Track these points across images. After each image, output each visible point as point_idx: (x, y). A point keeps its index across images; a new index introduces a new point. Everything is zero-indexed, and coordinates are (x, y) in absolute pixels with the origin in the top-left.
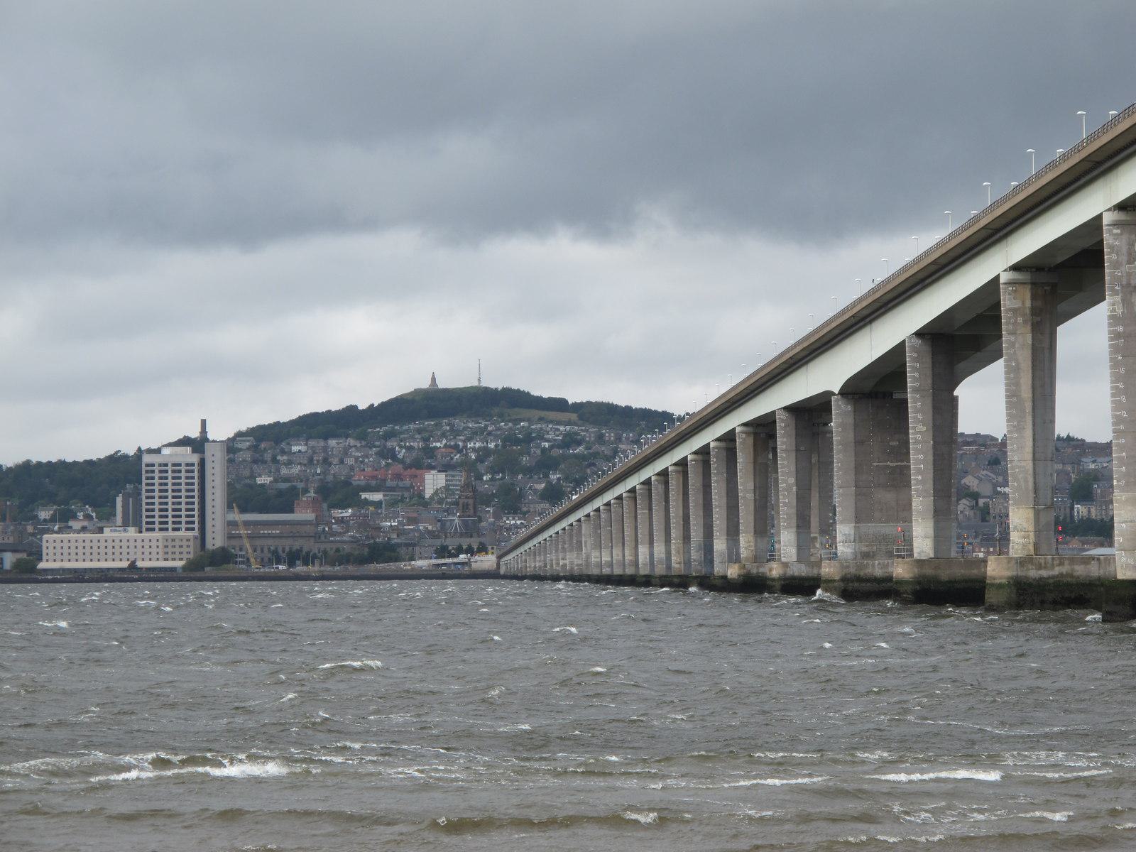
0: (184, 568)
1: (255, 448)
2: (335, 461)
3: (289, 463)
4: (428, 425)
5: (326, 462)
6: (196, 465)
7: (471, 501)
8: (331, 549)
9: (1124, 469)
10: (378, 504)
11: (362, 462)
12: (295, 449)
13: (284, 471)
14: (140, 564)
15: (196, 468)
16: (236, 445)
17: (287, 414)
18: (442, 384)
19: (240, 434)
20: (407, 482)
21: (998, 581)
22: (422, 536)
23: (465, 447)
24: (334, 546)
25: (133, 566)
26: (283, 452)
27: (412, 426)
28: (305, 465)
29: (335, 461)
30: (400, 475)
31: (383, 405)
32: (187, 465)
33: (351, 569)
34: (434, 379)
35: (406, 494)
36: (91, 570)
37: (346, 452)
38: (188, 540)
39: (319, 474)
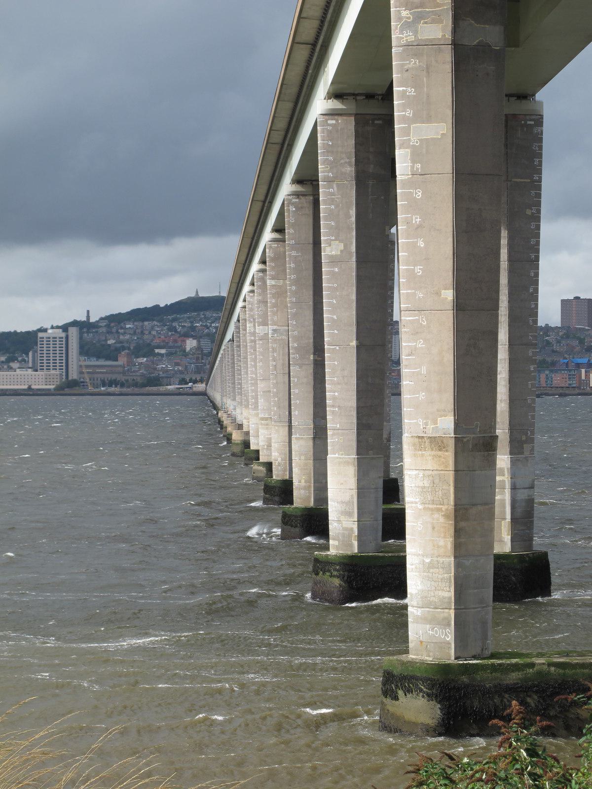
0: (55, 389)
1: (108, 326)
2: (147, 332)
3: (125, 333)
4: (194, 315)
5: (142, 333)
6: (64, 338)
7: (200, 356)
8: (131, 379)
9: (253, 400)
10: (162, 355)
11: (160, 333)
12: (128, 326)
13: (121, 337)
14: (33, 387)
15: (64, 340)
16: (99, 324)
17: (125, 309)
18: (202, 294)
19: (102, 319)
20: (179, 344)
21: (236, 442)
22: (176, 372)
23: (211, 326)
24: (132, 378)
25: (30, 388)
26: (122, 328)
27: (185, 315)
28: (132, 334)
29: (147, 332)
30: (176, 340)
31: (172, 305)
32: (60, 338)
33: (137, 390)
34: (197, 292)
35: (178, 350)
36: (10, 390)
37: (152, 328)
38: (57, 375)
39: (136, 340)
